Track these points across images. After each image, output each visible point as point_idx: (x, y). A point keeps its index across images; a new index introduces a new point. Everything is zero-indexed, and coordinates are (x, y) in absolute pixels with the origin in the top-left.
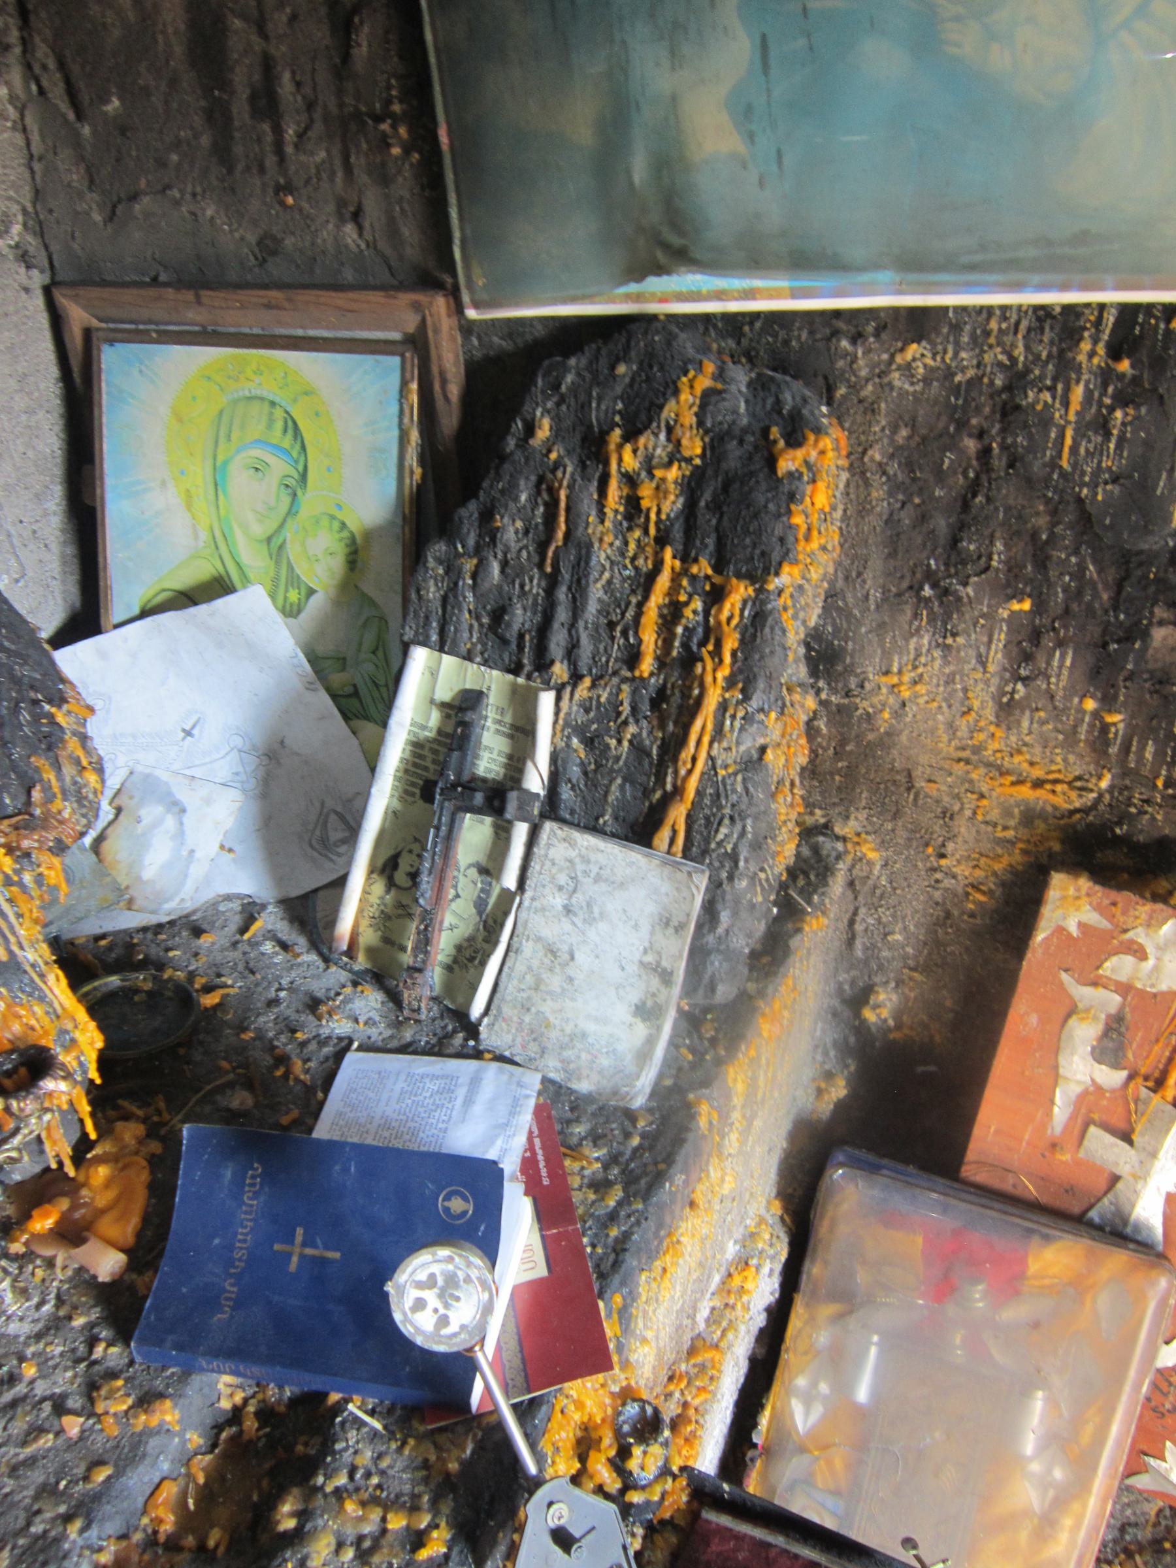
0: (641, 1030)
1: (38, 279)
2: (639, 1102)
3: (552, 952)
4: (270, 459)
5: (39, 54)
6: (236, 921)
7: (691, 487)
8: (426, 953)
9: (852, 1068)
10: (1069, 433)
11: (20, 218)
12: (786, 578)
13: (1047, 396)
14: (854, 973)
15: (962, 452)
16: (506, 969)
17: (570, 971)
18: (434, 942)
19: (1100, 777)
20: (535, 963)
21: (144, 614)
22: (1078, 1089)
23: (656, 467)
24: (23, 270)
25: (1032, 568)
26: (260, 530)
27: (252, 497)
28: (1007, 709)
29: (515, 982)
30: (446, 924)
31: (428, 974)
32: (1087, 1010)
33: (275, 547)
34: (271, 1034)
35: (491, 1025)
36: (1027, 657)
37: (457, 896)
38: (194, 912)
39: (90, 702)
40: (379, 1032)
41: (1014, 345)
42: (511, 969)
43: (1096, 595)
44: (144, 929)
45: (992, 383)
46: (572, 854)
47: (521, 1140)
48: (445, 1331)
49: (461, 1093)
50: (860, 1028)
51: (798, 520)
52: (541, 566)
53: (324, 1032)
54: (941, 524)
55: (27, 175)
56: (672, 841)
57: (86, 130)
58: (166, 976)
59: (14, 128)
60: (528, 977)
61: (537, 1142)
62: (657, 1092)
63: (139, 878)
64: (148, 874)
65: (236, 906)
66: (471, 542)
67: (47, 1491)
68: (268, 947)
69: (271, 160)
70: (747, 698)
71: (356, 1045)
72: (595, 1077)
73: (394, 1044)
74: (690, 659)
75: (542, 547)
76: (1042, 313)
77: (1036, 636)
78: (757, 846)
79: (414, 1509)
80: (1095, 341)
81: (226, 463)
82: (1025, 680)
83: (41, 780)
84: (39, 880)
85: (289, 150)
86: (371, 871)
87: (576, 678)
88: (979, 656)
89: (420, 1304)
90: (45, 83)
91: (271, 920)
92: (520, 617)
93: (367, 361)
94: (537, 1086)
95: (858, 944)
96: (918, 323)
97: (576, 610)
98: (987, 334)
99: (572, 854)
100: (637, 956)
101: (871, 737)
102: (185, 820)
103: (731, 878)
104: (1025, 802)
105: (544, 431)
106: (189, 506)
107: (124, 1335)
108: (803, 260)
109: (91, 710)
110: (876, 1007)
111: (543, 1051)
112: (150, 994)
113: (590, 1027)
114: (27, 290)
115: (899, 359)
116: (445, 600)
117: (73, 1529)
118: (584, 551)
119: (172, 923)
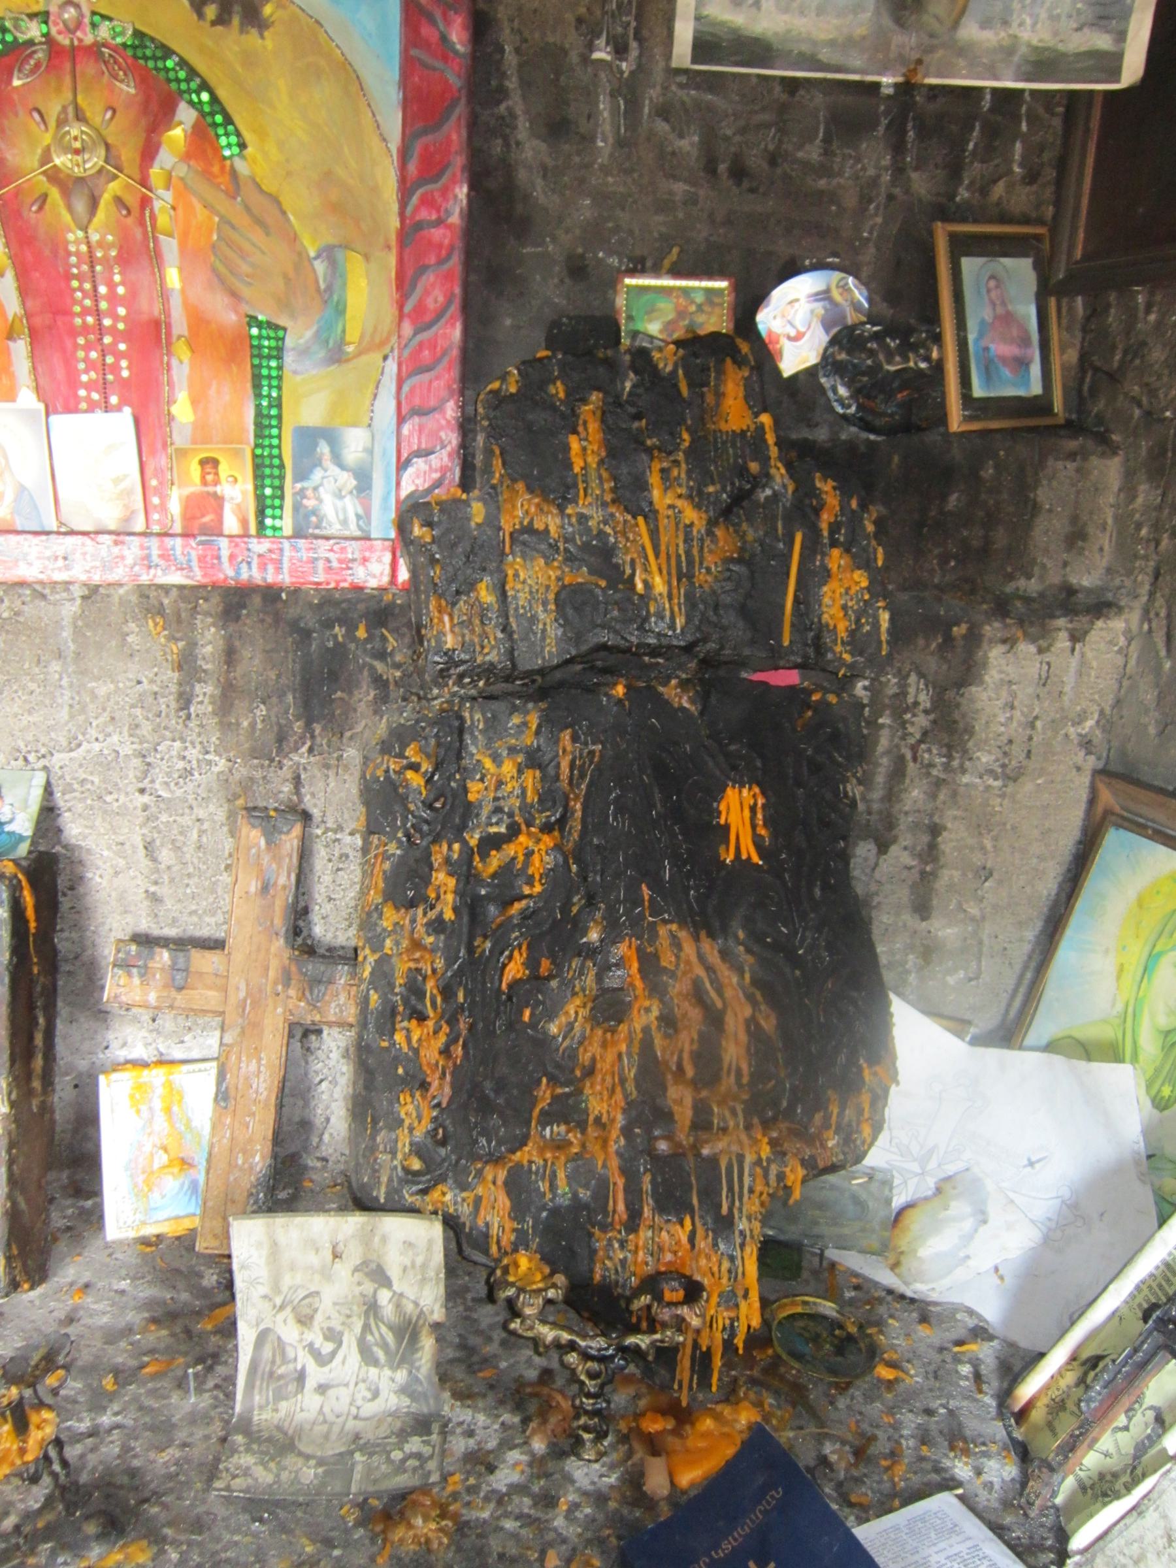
1: (1091, 762)
3: (1169, 1537)
5: (1157, 604)
6: (959, 1333)
8: (1066, 1457)
11: (1096, 716)
16: (1121, 1524)
18: (1079, 1453)
20: (1149, 1537)
24: (1082, 753)
29: (1123, 1542)
31: (1056, 1478)
34: (905, 1432)
37: (1126, 1428)
38: (936, 1304)
40: (984, 1499)
42: (1127, 1527)
44: (890, 1292)
53: (947, 1463)
55: (1116, 687)
57: (1168, 665)
58: (869, 1331)
59: (1120, 652)
60: (1136, 1545)
63: (915, 1251)
64: (924, 1252)
65: (971, 1322)
68: (965, 1369)
71: (960, 1491)
73: (993, 1518)
81: (1160, 954)
83: (826, 1108)
86: (1073, 1358)
90: (1154, 625)
91: (986, 1352)
102: (981, 1229)
106: (1118, 978)
112: (850, 1338)
114: (1079, 769)
119: (913, 1301)
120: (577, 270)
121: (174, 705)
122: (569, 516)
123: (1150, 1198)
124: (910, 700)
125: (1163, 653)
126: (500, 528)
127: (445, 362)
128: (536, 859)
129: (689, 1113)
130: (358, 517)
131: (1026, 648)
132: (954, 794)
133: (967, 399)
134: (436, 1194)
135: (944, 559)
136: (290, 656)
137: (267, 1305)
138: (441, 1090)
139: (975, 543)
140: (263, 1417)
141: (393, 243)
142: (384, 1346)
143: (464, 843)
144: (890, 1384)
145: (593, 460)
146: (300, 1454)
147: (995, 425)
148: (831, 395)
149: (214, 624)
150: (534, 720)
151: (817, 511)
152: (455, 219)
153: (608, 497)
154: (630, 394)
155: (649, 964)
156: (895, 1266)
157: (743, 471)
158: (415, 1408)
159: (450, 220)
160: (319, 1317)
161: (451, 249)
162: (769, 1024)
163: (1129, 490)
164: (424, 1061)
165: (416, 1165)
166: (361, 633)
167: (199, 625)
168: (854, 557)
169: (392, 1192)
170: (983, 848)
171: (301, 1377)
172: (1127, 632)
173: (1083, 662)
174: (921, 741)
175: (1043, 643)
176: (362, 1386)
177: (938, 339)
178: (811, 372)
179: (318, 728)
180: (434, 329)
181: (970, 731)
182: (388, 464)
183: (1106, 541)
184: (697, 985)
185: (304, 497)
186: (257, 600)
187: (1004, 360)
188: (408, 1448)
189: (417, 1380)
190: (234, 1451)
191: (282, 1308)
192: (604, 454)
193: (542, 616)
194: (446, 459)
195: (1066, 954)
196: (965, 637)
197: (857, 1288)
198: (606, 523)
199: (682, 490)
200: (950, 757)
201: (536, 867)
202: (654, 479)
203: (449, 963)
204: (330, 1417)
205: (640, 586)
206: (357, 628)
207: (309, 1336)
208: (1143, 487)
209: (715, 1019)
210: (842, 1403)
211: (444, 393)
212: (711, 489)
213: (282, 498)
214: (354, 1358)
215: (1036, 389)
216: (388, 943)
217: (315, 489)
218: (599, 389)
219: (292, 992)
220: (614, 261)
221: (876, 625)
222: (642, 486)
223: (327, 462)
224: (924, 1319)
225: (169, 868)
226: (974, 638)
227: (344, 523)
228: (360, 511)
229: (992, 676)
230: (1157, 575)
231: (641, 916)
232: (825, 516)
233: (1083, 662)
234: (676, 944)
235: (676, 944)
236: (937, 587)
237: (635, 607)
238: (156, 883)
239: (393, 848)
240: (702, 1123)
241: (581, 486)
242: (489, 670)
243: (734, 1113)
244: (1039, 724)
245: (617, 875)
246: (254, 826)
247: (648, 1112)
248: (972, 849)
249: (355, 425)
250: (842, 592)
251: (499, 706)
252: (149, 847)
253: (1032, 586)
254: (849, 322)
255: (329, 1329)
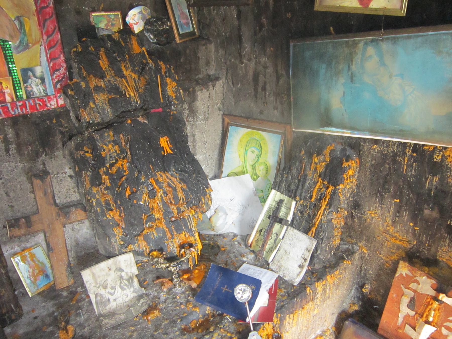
0: (299, 270)
1: (221, 113)
2: (296, 284)
4: (255, 150)
6: (232, 237)
7: (327, 167)
9: (360, 304)
10: (405, 166)
12: (341, 186)
13: (401, 159)
14: (362, 280)
15: (385, 168)
17: (288, 256)
19: (414, 241)
21: (228, 176)
22: (405, 314)
23: (320, 163)
25: (398, 194)
26: (251, 163)
27: (251, 157)
28: (394, 223)
30: (268, 243)
32: (406, 295)
33: (253, 167)
35: (272, 264)
36: (398, 212)
39: (212, 189)
41: (394, 148)
43: (412, 201)
44: (215, 235)
45: (390, 155)
46: (293, 233)
47: (271, 285)
48: (242, 299)
49: (262, 274)
50: (362, 293)
51: (345, 176)
52: (298, 178)
54: (381, 181)
56: (312, 234)
61: (274, 286)
62: (300, 283)
64: (217, 225)
65: (232, 234)
66: (287, 172)
67: (177, 315)
68: (236, 243)
69: (263, 98)
70: (330, 208)
72: (288, 277)
74: (321, 199)
75: (299, 174)
76: (400, 143)
77: (400, 207)
78: (328, 238)
79: (233, 333)
80: (409, 149)
81: (247, 150)
82: (398, 217)
84: (198, 216)
85: (267, 97)
86: (257, 231)
87: (301, 200)
88: (389, 210)
89: (239, 293)
91: (238, 238)
92: (293, 187)
93: (275, 135)
94: (277, 277)
95: (362, 272)
96: (376, 142)
97: (303, 186)
98: (389, 145)
99: (293, 233)
100: (301, 255)
101: (366, 224)
103: (321, 243)
104: (398, 244)
105: (303, 153)
107: (193, 297)
108: (352, 128)
109: (212, 190)
110: (365, 288)
111: (280, 271)
112: (213, 246)
113: (290, 268)
115: (372, 148)
116: (280, 181)
117: (179, 321)
118: (306, 176)
119: (220, 235)
120: (78, 12)
121: (4, 153)
122: (106, 81)
123: (258, 199)
124: (184, 108)
125: (232, 86)
126: (90, 88)
127: (58, 44)
128: (124, 166)
129: (176, 211)
130: (44, 90)
131: (205, 91)
132: (196, 127)
133: (179, 34)
134: (129, 247)
135: (182, 73)
136: (35, 132)
137: (95, 288)
138: (122, 224)
139: (188, 68)
140: (103, 312)
141: (35, 13)
142: (126, 285)
143: (106, 167)
144: (225, 251)
145: (107, 66)
146: (118, 314)
147: (186, 40)
148: (148, 37)
149: (10, 128)
150: (111, 133)
151: (161, 69)
152: (51, 5)
153: (113, 75)
154: (110, 47)
155: (157, 182)
156: (213, 230)
157: (142, 63)
158: (137, 294)
159: (50, 6)
160: (109, 285)
161: (52, 13)
162: (185, 187)
163: (217, 51)
164: (116, 219)
165: (122, 243)
166: (54, 121)
167: (7, 129)
168: (171, 79)
169: (119, 250)
170: (204, 137)
171: (109, 300)
172: (223, 83)
173: (216, 91)
174: (188, 116)
175: (208, 89)
176: (123, 295)
177: (169, 19)
178: (142, 32)
179: (47, 149)
180: (53, 36)
181: (197, 112)
182: (48, 74)
183: (213, 63)
184: (168, 183)
185: (28, 88)
186: (21, 119)
187: (184, 24)
188: (141, 302)
189: (135, 289)
190: (102, 321)
191: (99, 287)
192: (109, 63)
193: (106, 107)
194: (64, 71)
195: (227, 155)
196: (192, 91)
197: (208, 237)
198: (115, 81)
199: (130, 70)
200: (194, 119)
201: (125, 168)
202: (123, 68)
203: (113, 196)
204: (119, 305)
205: (128, 96)
206: (53, 120)
207: (107, 290)
208: (220, 51)
209: (175, 189)
210: (218, 258)
211: (59, 53)
212: (136, 68)
213: (21, 89)
214: (120, 290)
215: (192, 30)
216: (97, 196)
217: (30, 85)
218: (102, 47)
219: (61, 218)
220: (87, 9)
221: (180, 93)
222: (121, 71)
223: (32, 77)
224: (224, 237)
225: (14, 197)
226: (194, 91)
227: (40, 92)
228: (44, 89)
229: (199, 98)
230: (227, 70)
231: (152, 172)
232: (163, 70)
233: (216, 91)
234: (162, 176)
235: (162, 176)
236: (182, 80)
237: (129, 101)
238: (11, 202)
239: (89, 173)
240: (179, 212)
241: (106, 73)
242: (98, 124)
243: (185, 208)
244: (210, 107)
245: (143, 164)
246: (37, 179)
247: (167, 213)
248: (202, 138)
249: (37, 66)
250: (171, 88)
251: (101, 132)
252: (7, 194)
253: (201, 76)
254: (147, 18)
255: (112, 287)
